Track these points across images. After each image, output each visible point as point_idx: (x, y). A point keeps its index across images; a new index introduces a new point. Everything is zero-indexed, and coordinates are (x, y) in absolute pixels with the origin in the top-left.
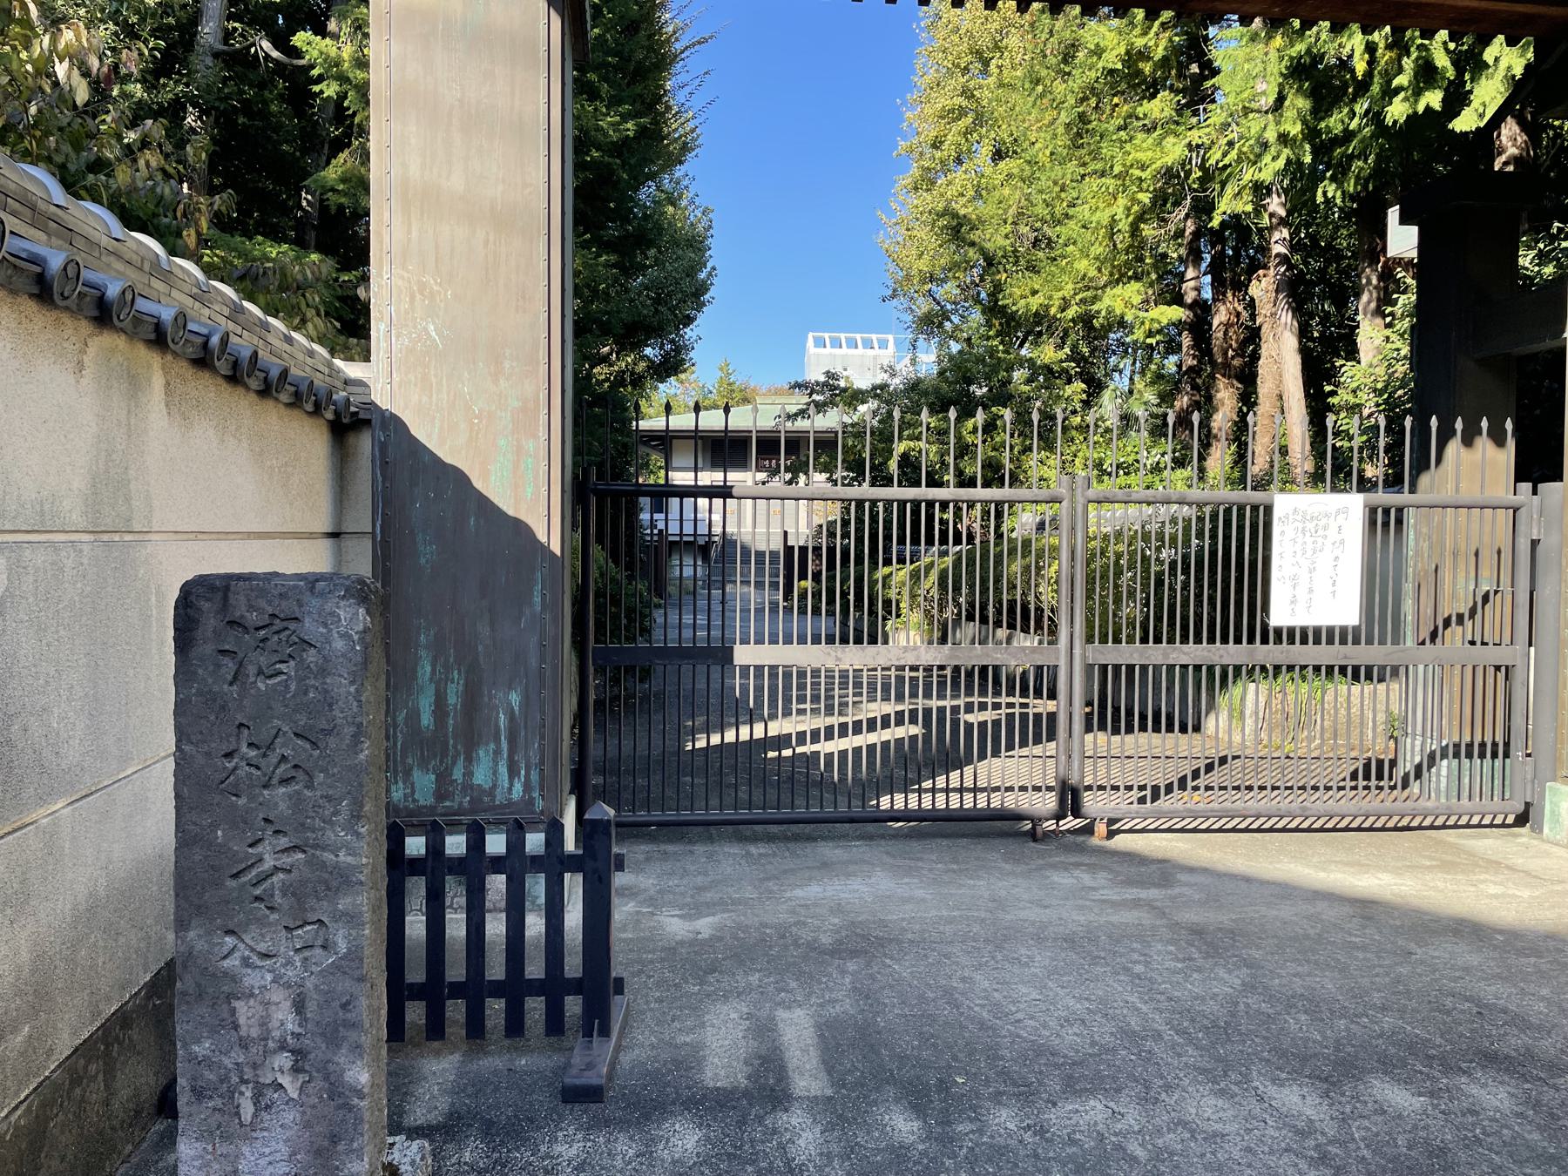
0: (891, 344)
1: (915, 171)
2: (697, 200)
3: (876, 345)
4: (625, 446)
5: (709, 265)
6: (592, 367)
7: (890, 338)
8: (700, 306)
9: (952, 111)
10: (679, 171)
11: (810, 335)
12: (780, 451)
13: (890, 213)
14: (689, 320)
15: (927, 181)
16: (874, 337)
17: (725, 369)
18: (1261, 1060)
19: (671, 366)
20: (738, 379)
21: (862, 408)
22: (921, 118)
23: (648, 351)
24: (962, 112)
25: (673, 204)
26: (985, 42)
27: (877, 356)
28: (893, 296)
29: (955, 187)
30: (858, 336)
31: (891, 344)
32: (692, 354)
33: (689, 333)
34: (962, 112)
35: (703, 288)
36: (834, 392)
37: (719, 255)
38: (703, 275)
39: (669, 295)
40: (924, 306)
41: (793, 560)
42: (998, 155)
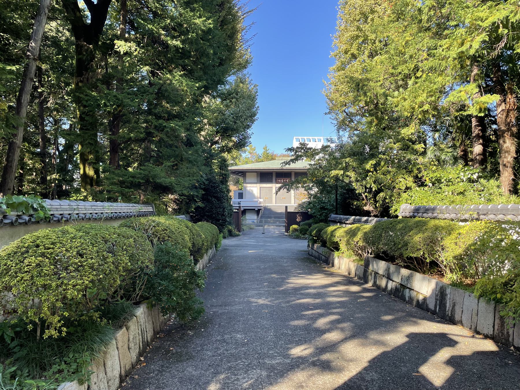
0: (322, 140)
1: (338, 64)
2: (252, 82)
3: (317, 140)
4: (225, 175)
5: (256, 106)
6: (212, 145)
7: (322, 138)
8: (253, 122)
9: (353, 37)
10: (245, 71)
11: (295, 137)
12: (284, 177)
13: (328, 80)
14: (248, 127)
15: (342, 68)
16: (316, 138)
17: (265, 148)
18: (327, 209)
19: (240, 145)
20: (270, 152)
21: (317, 157)
22: (340, 42)
23: (233, 138)
24: (358, 37)
25: (242, 83)
26: (366, 9)
27: (322, 135)
28: (329, 113)
29: (355, 69)
30: (311, 138)
31: (322, 140)
32: (250, 140)
33: (249, 131)
34: (358, 37)
35: (254, 115)
36: (304, 151)
37: (261, 103)
38: (254, 110)
39: (241, 116)
40: (341, 117)
41: (290, 217)
42: (371, 56)
